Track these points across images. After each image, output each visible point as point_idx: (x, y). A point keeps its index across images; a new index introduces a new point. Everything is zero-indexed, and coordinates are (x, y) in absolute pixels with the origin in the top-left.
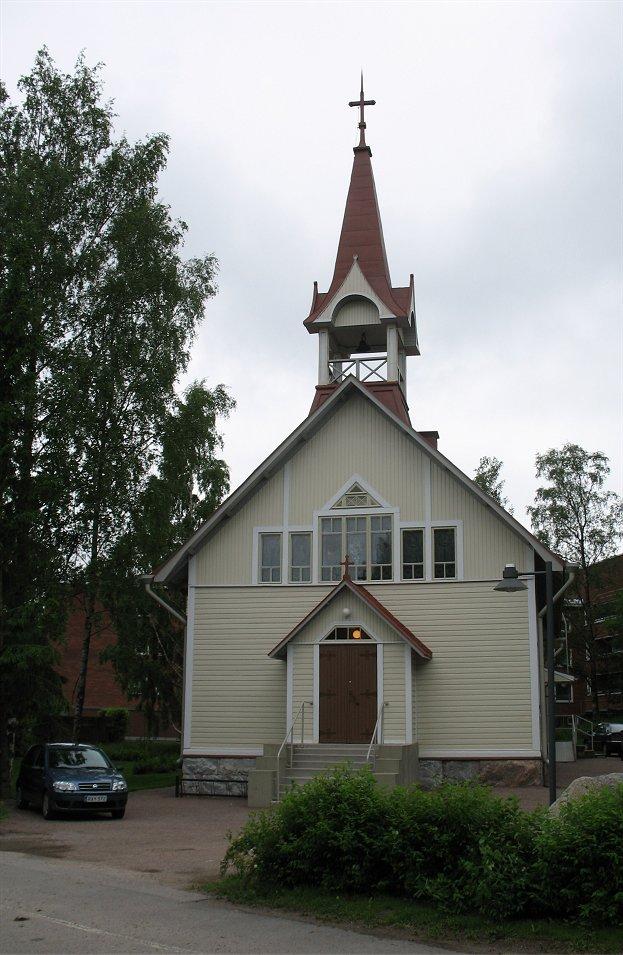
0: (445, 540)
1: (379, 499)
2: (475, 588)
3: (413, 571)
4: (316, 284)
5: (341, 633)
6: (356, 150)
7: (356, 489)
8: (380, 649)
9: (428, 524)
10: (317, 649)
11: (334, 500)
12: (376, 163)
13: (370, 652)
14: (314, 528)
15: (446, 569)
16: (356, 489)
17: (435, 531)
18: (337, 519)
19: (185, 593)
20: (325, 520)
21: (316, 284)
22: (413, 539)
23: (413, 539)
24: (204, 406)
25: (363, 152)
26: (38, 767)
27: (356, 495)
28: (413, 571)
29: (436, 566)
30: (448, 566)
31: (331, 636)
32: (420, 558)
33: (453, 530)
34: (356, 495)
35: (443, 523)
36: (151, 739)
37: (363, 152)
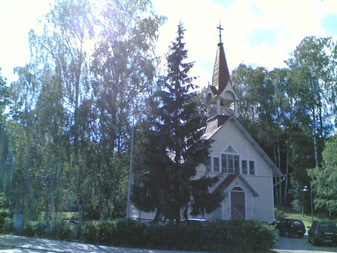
0: (252, 163)
1: (236, 150)
3: (245, 172)
5: (235, 188)
6: (218, 45)
7: (230, 147)
9: (248, 160)
11: (224, 150)
13: (243, 194)
14: (220, 157)
15: (252, 172)
16: (230, 147)
17: (250, 162)
18: (226, 155)
19: (265, 150)
20: (223, 155)
22: (244, 162)
23: (244, 162)
24: (168, 88)
26: (98, 120)
27: (230, 149)
28: (245, 172)
31: (233, 189)
32: (246, 168)
34: (230, 149)
36: (5, 190)
37: (221, 45)
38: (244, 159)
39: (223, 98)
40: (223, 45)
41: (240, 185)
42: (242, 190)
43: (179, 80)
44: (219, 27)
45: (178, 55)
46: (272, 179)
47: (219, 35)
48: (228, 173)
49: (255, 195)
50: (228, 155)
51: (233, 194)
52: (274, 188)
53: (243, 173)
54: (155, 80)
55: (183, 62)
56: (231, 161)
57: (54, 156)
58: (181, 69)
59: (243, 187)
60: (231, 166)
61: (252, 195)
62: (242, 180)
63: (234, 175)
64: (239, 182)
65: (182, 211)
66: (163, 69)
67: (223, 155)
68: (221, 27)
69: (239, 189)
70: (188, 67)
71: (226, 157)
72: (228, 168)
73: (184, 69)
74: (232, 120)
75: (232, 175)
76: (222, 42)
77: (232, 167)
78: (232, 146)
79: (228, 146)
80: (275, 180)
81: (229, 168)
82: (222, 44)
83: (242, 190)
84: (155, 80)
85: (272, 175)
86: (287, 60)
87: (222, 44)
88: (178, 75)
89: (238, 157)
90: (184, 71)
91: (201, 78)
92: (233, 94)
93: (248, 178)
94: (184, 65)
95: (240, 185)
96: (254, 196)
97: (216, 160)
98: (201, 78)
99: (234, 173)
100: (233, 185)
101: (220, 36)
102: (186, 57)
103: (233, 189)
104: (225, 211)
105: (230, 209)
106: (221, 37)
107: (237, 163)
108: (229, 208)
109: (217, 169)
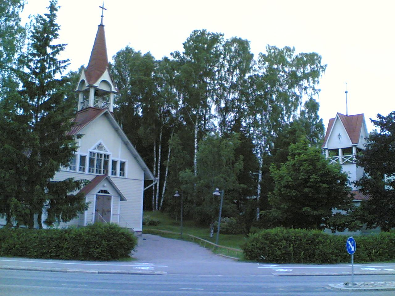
0: (123, 164)
1: (107, 150)
2: (130, 181)
3: (114, 173)
4: (100, 7)
5: (102, 191)
8: (112, 197)
9: (119, 160)
10: (95, 196)
12: (106, 29)
13: (109, 198)
15: (122, 174)
16: (100, 144)
17: (121, 162)
18: (94, 153)
20: (91, 153)
21: (100, 7)
22: (114, 162)
25: (101, 26)
27: (100, 147)
28: (114, 173)
29: (89, 169)
30: (83, 168)
31: (99, 192)
33: (121, 162)
34: (100, 147)
35: (123, 160)
37: (101, 26)
38: (115, 159)
39: (97, 88)
40: (105, 27)
41: (108, 188)
42: (108, 193)
43: (45, 63)
44: (102, 6)
45: (46, 31)
46: (143, 182)
47: (101, 15)
48: (95, 173)
49: (122, 199)
50: (98, 154)
51: (98, 197)
52: (145, 192)
53: (112, 174)
54: (16, 56)
55: (53, 42)
56: (99, 161)
57: (12, 6)
58: (49, 51)
59: (112, 193)
60: (99, 166)
61: (120, 199)
62: (110, 183)
63: (103, 176)
64: (105, 185)
65: (36, 216)
66: (26, 46)
67: (91, 153)
68: (104, 7)
69: (106, 192)
70: (59, 49)
71: (94, 156)
72: (95, 168)
73: (52, 51)
74: (106, 114)
75: (100, 176)
76: (104, 24)
77: (100, 167)
78: (103, 144)
79: (97, 143)
80: (147, 182)
81: (97, 167)
82: (104, 26)
83: (108, 193)
84: (16, 56)
85: (143, 178)
86: (173, 52)
87: (104, 26)
88: (45, 58)
89: (108, 156)
90: (52, 53)
91: (74, 56)
92: (110, 85)
93: (117, 181)
94: (53, 47)
95: (108, 188)
96: (121, 200)
97: (83, 158)
98: (74, 56)
99: (102, 174)
100: (99, 187)
101: (102, 16)
102: (56, 36)
103: (99, 192)
104: (89, 217)
105: (94, 215)
106: (103, 17)
107: (106, 163)
108: (93, 213)
109: (82, 169)
